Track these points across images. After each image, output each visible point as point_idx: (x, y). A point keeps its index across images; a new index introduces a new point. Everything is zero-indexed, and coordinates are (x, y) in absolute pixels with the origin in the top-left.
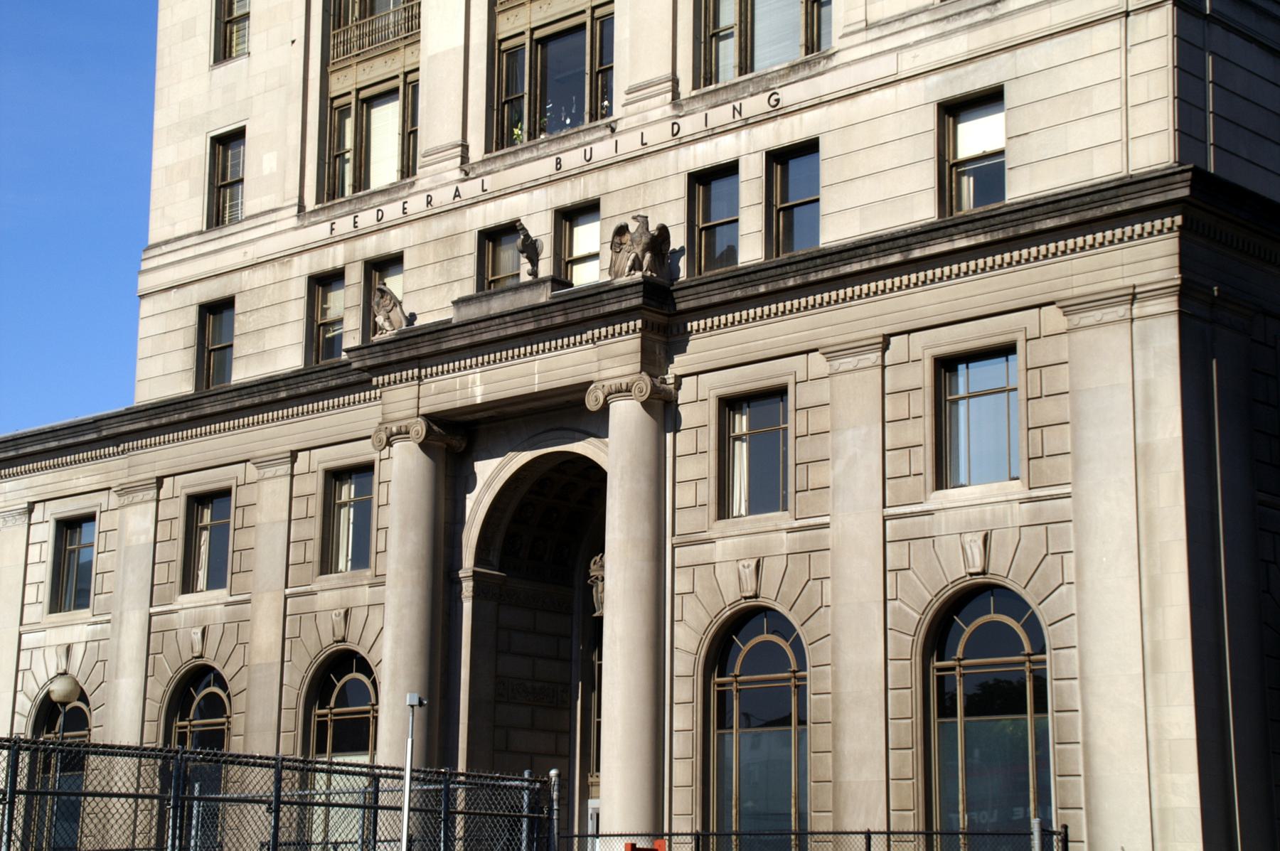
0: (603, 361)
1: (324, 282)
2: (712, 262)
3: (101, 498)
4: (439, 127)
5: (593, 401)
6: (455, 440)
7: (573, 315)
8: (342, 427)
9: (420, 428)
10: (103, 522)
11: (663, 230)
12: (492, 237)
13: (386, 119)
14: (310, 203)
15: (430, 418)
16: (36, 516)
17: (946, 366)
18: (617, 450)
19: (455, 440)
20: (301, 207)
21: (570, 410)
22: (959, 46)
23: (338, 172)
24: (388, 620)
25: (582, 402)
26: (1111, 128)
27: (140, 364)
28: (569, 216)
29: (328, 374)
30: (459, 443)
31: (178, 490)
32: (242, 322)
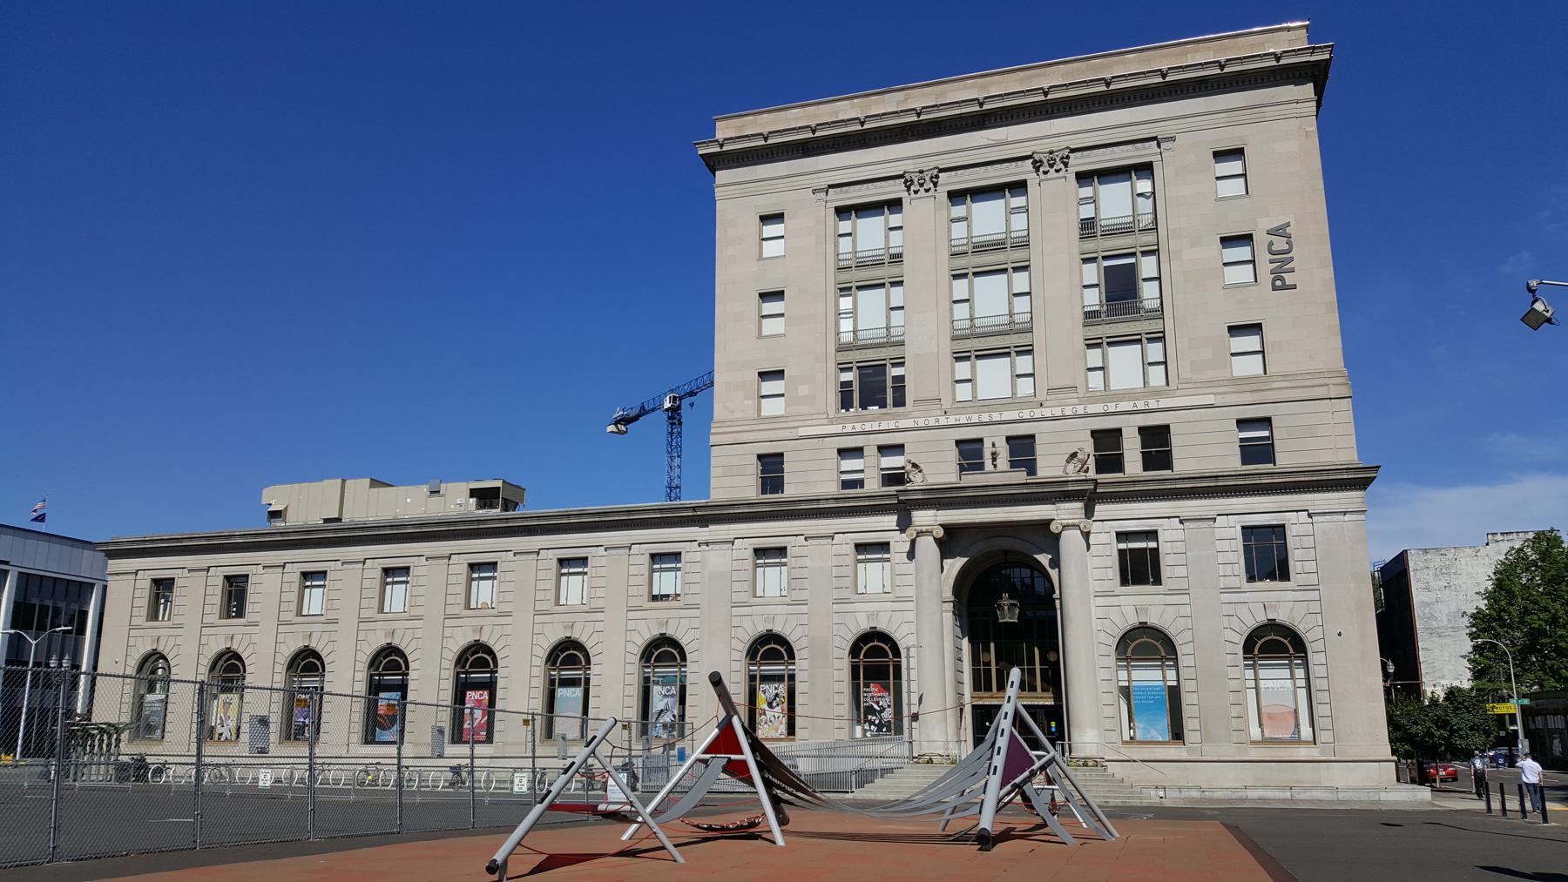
0: (1064, 514)
22: (1248, 398)
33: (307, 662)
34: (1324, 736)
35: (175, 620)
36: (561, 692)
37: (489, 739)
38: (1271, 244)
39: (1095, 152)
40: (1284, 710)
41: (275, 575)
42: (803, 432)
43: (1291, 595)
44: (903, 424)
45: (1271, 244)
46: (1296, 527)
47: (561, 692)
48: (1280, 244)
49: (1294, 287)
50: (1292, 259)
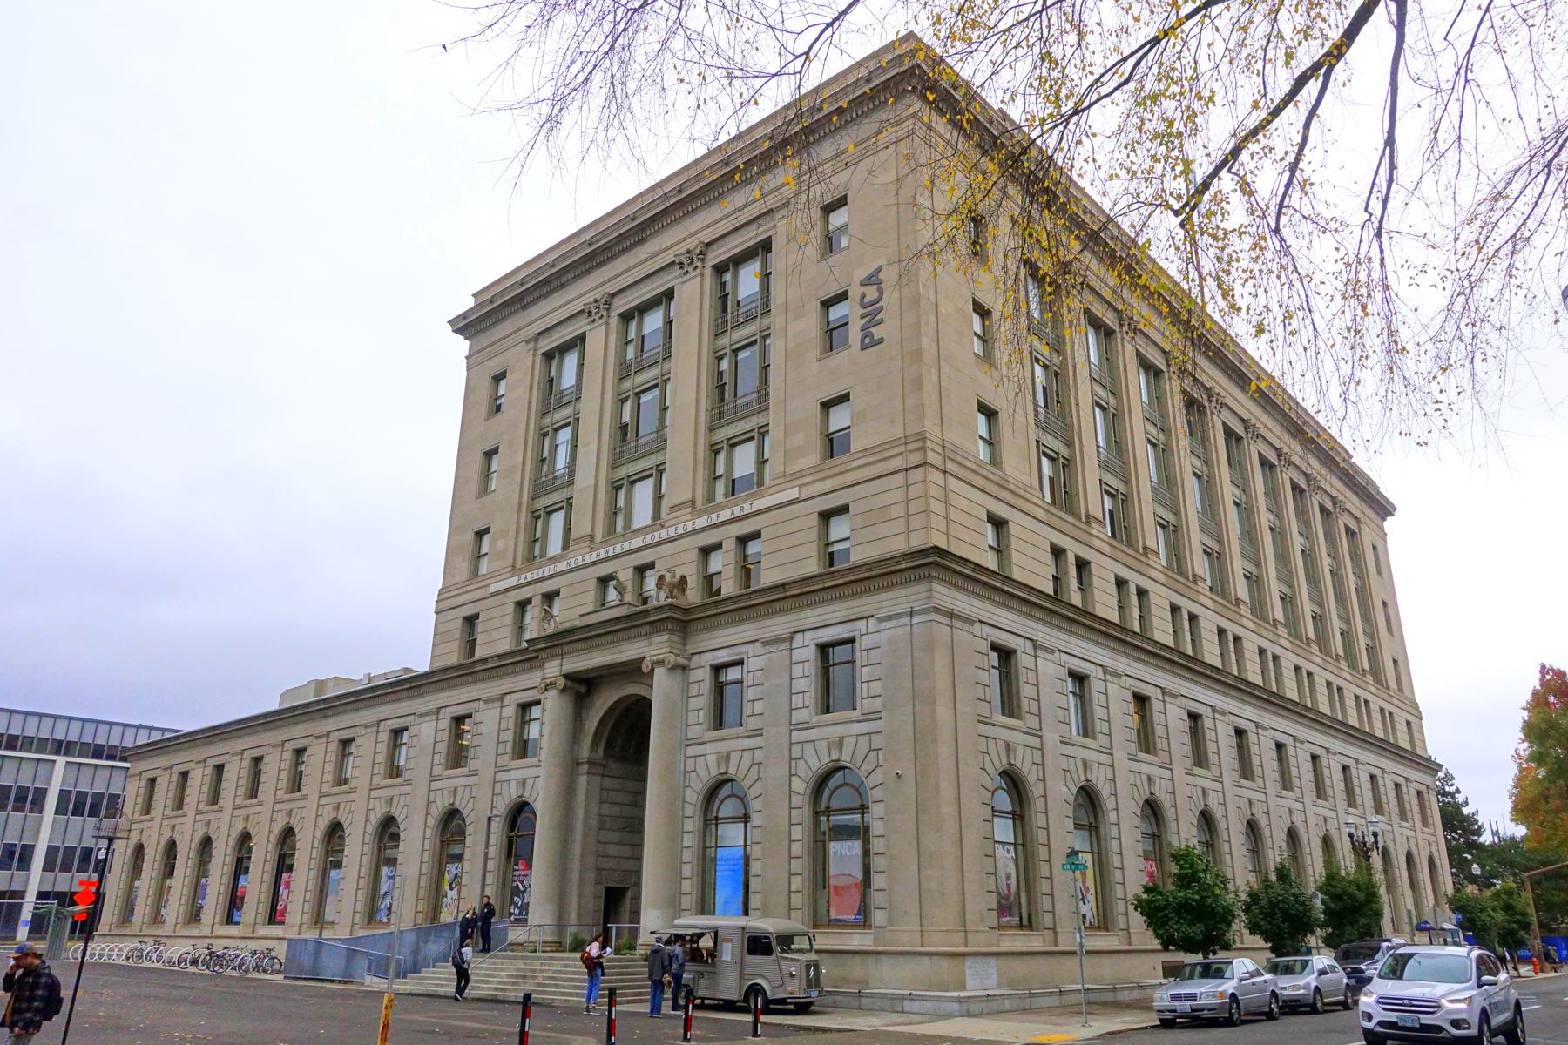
0: (653, 648)
1: (522, 605)
2: (712, 595)
3: (750, 647)
4: (581, 527)
5: (645, 668)
6: (582, 687)
7: (638, 621)
8: (525, 683)
9: (561, 682)
10: (477, 717)
11: (683, 579)
12: (604, 581)
13: (644, 491)
14: (519, 565)
15: (567, 676)
16: (506, 702)
17: (824, 649)
18: (661, 689)
19: (582, 687)
20: (513, 566)
21: (633, 670)
22: (829, 484)
23: (533, 548)
24: (539, 781)
25: (640, 669)
26: (900, 525)
27: (815, 552)
28: (641, 570)
29: (528, 656)
30: (583, 689)
31: (290, 746)
32: (480, 626)
33: (335, 830)
34: (878, 917)
35: (752, 723)
36: (835, 847)
37: (863, 919)
38: (863, 296)
39: (628, 292)
40: (849, 881)
41: (779, 655)
42: (492, 589)
43: (856, 728)
44: (759, 504)
45: (863, 296)
46: (870, 636)
47: (835, 847)
48: (872, 293)
49: (881, 341)
50: (881, 309)
